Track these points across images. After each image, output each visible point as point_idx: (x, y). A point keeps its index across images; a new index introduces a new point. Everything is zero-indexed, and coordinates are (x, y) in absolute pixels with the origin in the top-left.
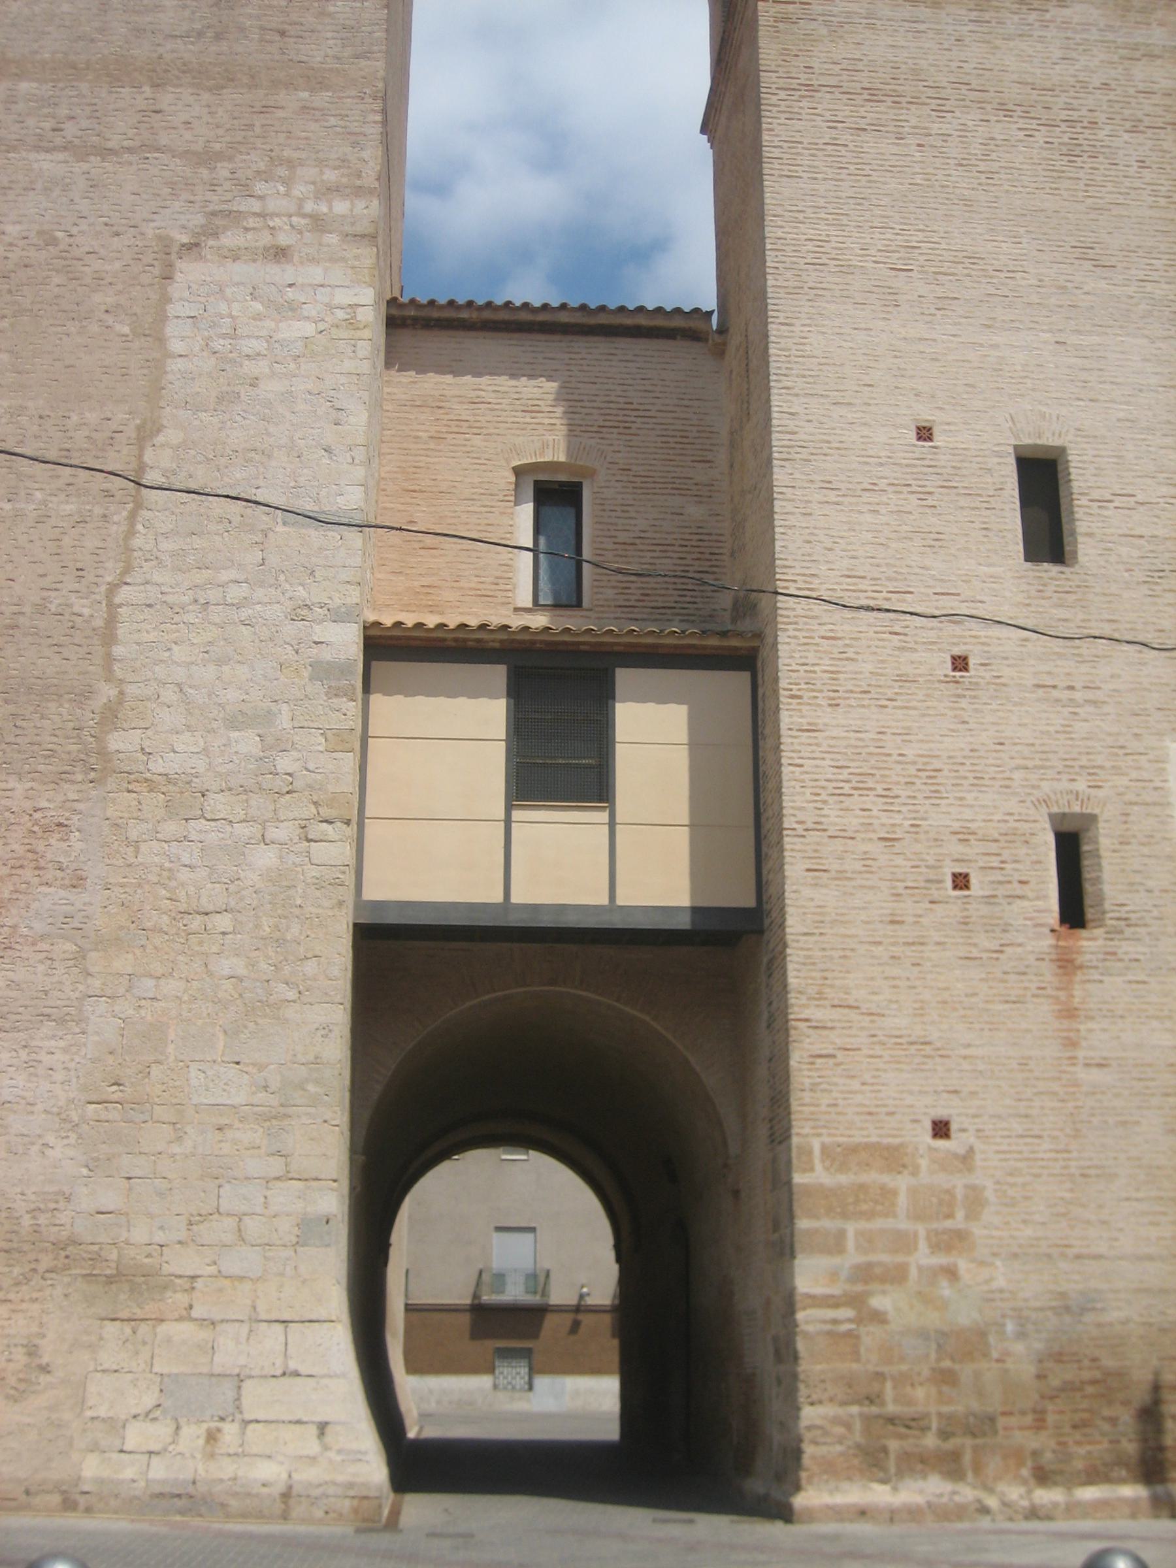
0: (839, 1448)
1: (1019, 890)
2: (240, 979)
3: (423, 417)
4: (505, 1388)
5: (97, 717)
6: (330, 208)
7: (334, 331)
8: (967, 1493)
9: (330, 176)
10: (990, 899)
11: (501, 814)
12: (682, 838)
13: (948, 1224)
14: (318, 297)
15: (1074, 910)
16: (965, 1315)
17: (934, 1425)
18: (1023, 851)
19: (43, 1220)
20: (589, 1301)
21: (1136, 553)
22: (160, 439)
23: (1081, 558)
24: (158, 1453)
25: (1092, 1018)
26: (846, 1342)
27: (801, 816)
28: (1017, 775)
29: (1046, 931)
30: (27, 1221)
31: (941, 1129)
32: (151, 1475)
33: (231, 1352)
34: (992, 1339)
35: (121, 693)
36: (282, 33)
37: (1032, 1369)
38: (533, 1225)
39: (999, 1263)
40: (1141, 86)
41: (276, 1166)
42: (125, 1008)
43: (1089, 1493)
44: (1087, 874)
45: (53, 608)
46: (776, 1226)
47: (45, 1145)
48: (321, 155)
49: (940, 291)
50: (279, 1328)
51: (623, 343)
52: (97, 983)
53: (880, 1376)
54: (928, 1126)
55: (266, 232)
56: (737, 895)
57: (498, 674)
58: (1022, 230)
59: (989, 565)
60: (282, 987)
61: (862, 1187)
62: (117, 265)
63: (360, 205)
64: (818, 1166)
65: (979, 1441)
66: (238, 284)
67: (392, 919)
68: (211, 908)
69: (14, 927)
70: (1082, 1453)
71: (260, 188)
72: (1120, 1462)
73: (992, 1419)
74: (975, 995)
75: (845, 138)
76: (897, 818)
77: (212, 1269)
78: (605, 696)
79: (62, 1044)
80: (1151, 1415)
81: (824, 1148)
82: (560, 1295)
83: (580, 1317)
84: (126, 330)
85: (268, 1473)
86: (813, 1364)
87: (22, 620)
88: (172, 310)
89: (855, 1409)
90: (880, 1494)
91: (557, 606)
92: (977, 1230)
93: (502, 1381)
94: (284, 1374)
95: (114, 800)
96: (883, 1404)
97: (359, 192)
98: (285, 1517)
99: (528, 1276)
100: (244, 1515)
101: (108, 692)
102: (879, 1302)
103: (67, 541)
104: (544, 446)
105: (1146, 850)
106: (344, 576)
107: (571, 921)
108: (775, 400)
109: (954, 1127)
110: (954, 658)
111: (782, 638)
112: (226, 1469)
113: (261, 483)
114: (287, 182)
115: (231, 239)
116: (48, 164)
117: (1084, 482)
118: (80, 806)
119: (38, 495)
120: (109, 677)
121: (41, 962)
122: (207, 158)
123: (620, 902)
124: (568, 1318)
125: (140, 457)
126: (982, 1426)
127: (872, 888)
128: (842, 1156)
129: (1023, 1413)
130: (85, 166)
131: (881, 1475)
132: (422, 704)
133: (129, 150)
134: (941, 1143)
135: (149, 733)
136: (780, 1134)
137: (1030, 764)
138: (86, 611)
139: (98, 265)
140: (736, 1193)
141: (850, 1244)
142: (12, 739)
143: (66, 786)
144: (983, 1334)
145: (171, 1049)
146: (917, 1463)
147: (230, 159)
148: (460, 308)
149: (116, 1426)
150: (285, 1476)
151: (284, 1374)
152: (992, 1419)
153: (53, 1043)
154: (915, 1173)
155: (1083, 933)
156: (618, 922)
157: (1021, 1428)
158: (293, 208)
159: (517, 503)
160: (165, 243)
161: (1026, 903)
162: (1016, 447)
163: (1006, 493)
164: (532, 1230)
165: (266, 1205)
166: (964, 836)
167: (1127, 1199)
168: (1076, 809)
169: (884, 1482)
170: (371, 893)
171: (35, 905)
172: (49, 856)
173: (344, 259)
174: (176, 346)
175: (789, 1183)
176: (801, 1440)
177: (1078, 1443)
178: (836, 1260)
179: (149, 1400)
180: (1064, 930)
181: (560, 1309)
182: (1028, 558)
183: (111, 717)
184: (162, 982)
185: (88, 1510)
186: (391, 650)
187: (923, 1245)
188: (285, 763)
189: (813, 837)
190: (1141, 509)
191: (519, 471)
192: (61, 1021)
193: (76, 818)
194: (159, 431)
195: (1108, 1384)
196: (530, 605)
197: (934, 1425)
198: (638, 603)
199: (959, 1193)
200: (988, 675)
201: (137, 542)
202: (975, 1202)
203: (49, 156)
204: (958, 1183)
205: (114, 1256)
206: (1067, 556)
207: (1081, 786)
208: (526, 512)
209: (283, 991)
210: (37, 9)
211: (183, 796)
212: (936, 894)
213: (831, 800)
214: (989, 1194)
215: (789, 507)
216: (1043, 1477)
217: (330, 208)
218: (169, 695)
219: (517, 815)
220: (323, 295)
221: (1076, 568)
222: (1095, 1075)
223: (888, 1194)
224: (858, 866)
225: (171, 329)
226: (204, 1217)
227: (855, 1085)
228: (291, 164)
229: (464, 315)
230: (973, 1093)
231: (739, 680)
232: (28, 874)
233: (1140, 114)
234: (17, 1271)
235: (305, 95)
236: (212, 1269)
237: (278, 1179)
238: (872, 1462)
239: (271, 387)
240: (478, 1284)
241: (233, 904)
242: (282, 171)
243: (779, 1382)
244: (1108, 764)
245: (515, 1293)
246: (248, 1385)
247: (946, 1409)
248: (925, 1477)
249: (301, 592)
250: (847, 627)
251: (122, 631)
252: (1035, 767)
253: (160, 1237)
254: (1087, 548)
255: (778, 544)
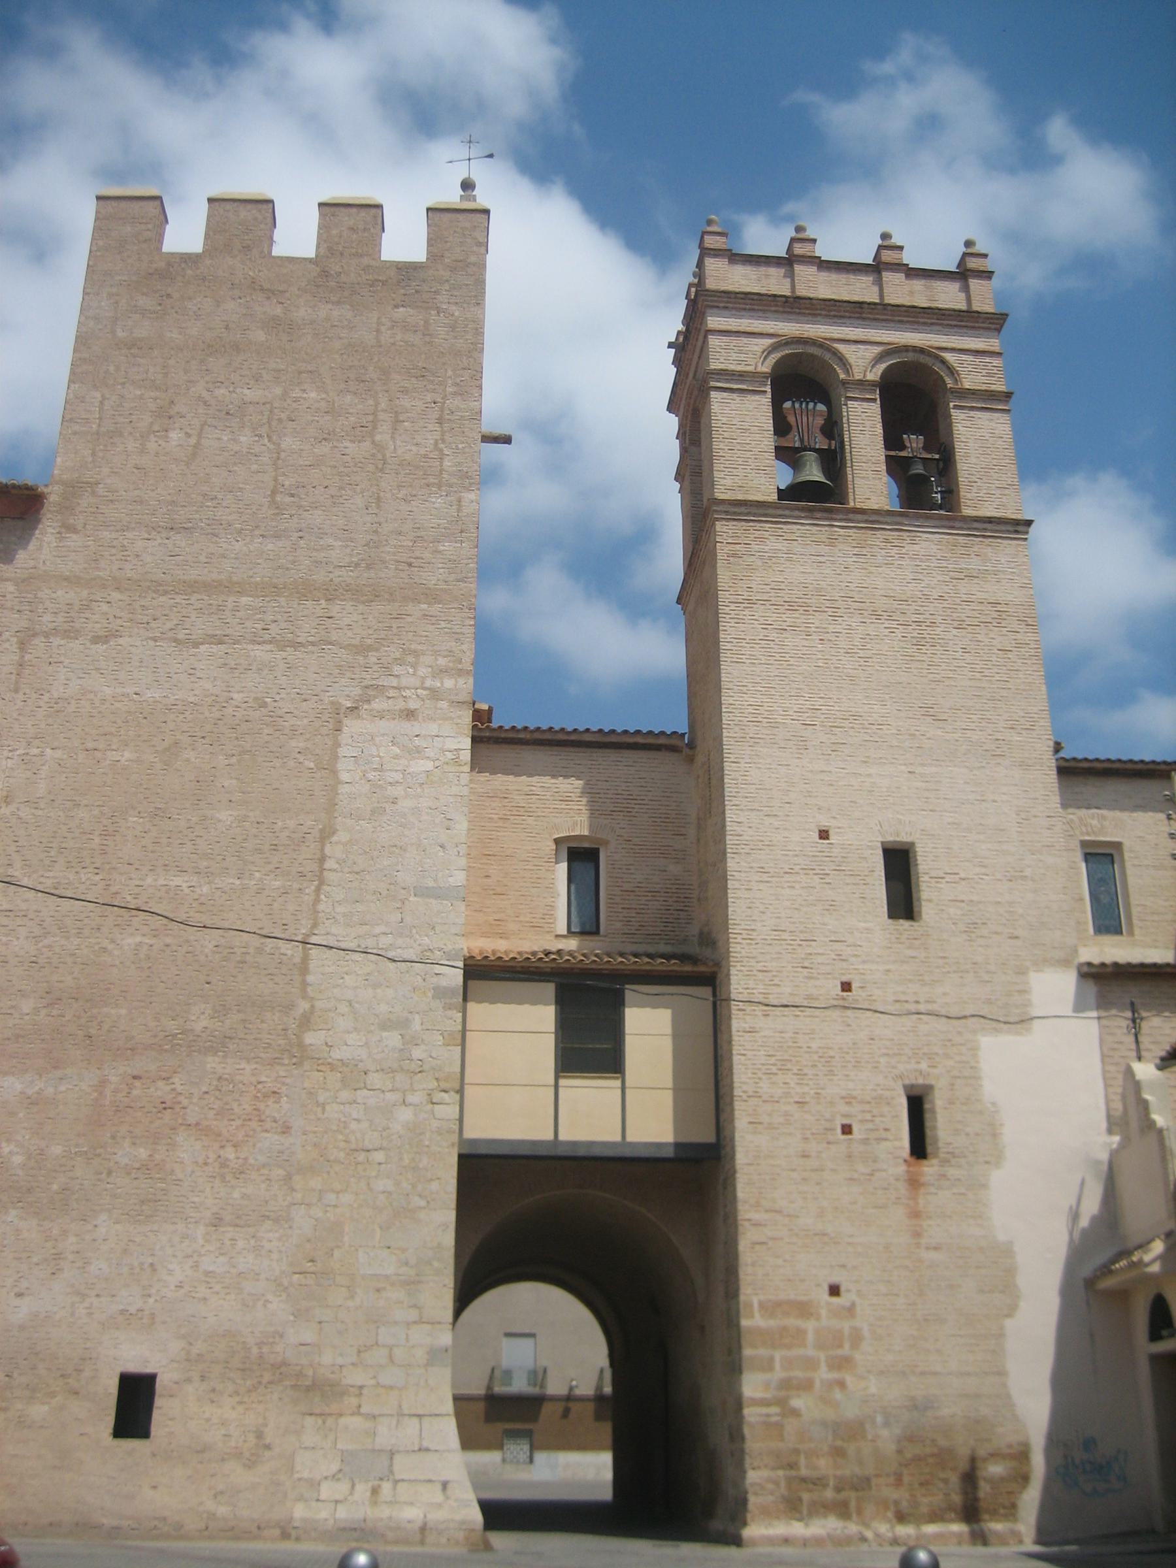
0: (771, 1498)
1: (884, 1134)
2: (390, 1193)
3: (494, 805)
4: (511, 1461)
5: (297, 1022)
6: (442, 683)
7: (445, 766)
8: (853, 1528)
9: (442, 662)
10: (865, 1141)
11: (552, 1081)
12: (668, 1098)
13: (839, 1352)
14: (435, 744)
15: (919, 1147)
16: (851, 1411)
17: (831, 1483)
18: (886, 1109)
19: (265, 1349)
20: (578, 1392)
21: (959, 912)
22: (335, 839)
23: (924, 916)
24: (341, 1502)
25: (930, 1218)
26: (775, 1429)
27: (745, 1088)
28: (882, 1060)
29: (901, 1161)
30: (255, 1350)
31: (834, 1290)
32: (337, 1516)
33: (386, 1436)
34: (868, 1426)
35: (313, 1006)
36: (410, 565)
37: (893, 1447)
38: (533, 1331)
39: (871, 1377)
40: (964, 597)
41: (413, 1315)
42: (317, 1212)
43: (930, 1529)
44: (928, 1124)
45: (268, 950)
46: (730, 1352)
47: (267, 1301)
48: (435, 648)
49: (833, 739)
50: (415, 1420)
51: (627, 753)
52: (299, 1196)
53: (797, 1452)
54: (826, 1288)
55: (401, 699)
56: (704, 1135)
57: (549, 989)
58: (887, 696)
59: (865, 922)
60: (417, 1198)
61: (785, 1328)
62: (305, 721)
63: (461, 681)
64: (757, 1314)
65: (860, 1494)
66: (383, 735)
67: (483, 1151)
68: (371, 1147)
69: (246, 1159)
70: (926, 1502)
71: (397, 670)
72: (950, 1508)
73: (868, 1479)
74: (855, 1203)
75: (774, 635)
76: (806, 1089)
77: (373, 1382)
78: (617, 1004)
79: (277, 1235)
80: (970, 1478)
81: (761, 1304)
82: (555, 1387)
83: (571, 1404)
84: (312, 765)
85: (412, 1514)
86: (755, 1443)
87: (248, 958)
88: (342, 751)
89: (781, 1473)
90: (797, 1529)
91: (583, 933)
92: (858, 1356)
93: (508, 1455)
94: (420, 1450)
95: (308, 1077)
96: (798, 1469)
97: (461, 672)
98: (422, 1542)
99: (530, 1372)
100: (396, 1542)
101: (304, 1006)
102: (797, 1403)
103: (276, 905)
104: (575, 823)
105: (965, 1108)
106: (454, 931)
107: (597, 1152)
108: (728, 814)
109: (842, 1289)
110: (843, 984)
111: (733, 971)
112: (384, 1512)
113: (400, 867)
114: (414, 666)
115: (378, 704)
116: (260, 653)
117: (926, 865)
118: (288, 1081)
119: (257, 875)
120: (305, 996)
121: (263, 1182)
122: (362, 649)
123: (629, 1139)
124: (559, 1407)
125: (322, 850)
126: (862, 1484)
127: (790, 1134)
128: (770, 1308)
129: (888, 1475)
130: (284, 654)
131: (797, 1515)
132: (501, 1009)
133: (313, 644)
134: (835, 1300)
135: (331, 1033)
136: (732, 1292)
137: (891, 1052)
138: (289, 952)
139: (293, 721)
140: (702, 1329)
141: (777, 1365)
142: (242, 1036)
143: (278, 1067)
144: (862, 1424)
145: (346, 1239)
146: (821, 1508)
147: (377, 650)
148: (518, 731)
149: (314, 1484)
150: (422, 1516)
151: (420, 1450)
152: (868, 1479)
153: (271, 1234)
154: (818, 1318)
155: (925, 1162)
156: (628, 1153)
157: (887, 1485)
158: (418, 684)
159: (557, 863)
160: (336, 709)
161: (888, 1144)
162: (882, 843)
163: (876, 874)
164: (533, 1335)
165: (407, 1339)
166: (848, 1100)
167: (954, 1336)
168: (921, 1081)
169: (800, 1520)
170: (469, 1134)
171: (259, 1145)
172: (267, 1113)
173: (451, 718)
174: (345, 777)
175: (738, 1325)
176: (746, 1493)
177: (924, 1495)
178: (768, 1376)
179: (335, 1467)
180: (912, 1160)
181: (553, 1399)
182: (891, 916)
183: (306, 1022)
184: (341, 1195)
185: (298, 1539)
186: (483, 973)
187: (823, 1367)
188: (417, 1053)
189: (754, 1101)
190: (963, 883)
191: (557, 841)
192: (276, 1221)
193: (284, 1088)
194: (334, 833)
195: (943, 1457)
196: (565, 933)
197: (831, 1483)
198: (639, 945)
199: (846, 1331)
200: (864, 994)
201: (321, 907)
202: (856, 1338)
203: (259, 647)
204: (846, 1326)
205: (310, 1373)
206: (915, 914)
207: (924, 1066)
208: (563, 867)
209: (418, 1202)
210: (252, 548)
211: (352, 1075)
212: (831, 1138)
213: (764, 1077)
214: (866, 1333)
215: (737, 885)
216: (901, 1518)
217: (442, 683)
218: (343, 1008)
219: (562, 1082)
220: (438, 742)
221: (922, 923)
222: (933, 1255)
223: (801, 1333)
224: (781, 1120)
225: (340, 766)
226: (368, 1348)
227: (780, 1262)
228: (415, 653)
229: (521, 736)
230: (855, 1267)
231: (705, 992)
232: (254, 1124)
233: (963, 616)
234: (249, 1383)
235: (425, 606)
236: (373, 1382)
237: (415, 1322)
238: (793, 1507)
239: (406, 804)
240: (491, 1378)
241: (385, 1145)
242: (411, 659)
243: (732, 1455)
244: (941, 1052)
245: (519, 1385)
246: (398, 1459)
247: (839, 1473)
248: (825, 1517)
249: (426, 940)
250: (774, 964)
251: (312, 965)
252: (895, 1054)
253: (340, 1361)
254: (928, 909)
255: (730, 909)
